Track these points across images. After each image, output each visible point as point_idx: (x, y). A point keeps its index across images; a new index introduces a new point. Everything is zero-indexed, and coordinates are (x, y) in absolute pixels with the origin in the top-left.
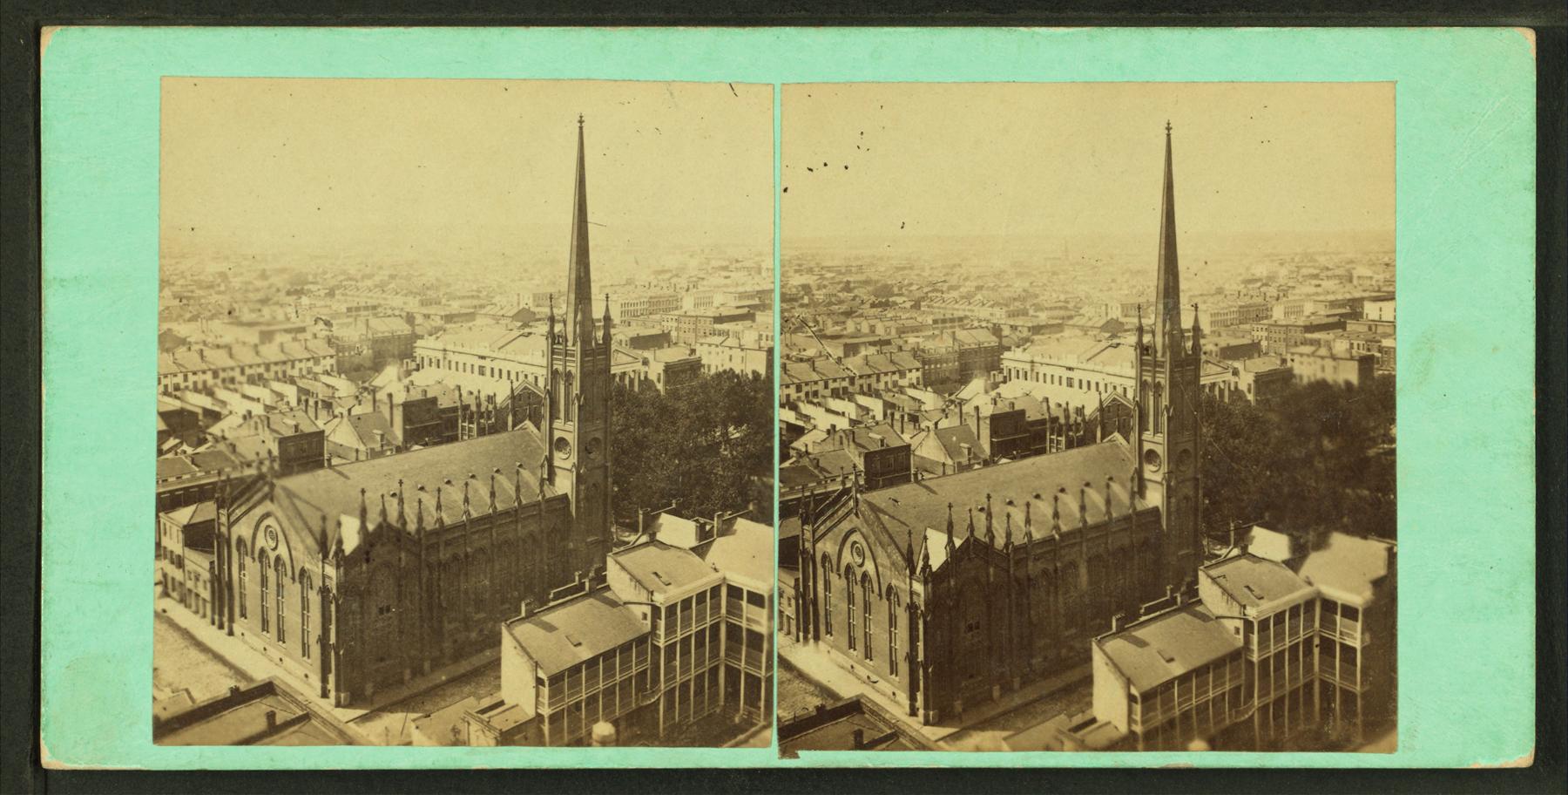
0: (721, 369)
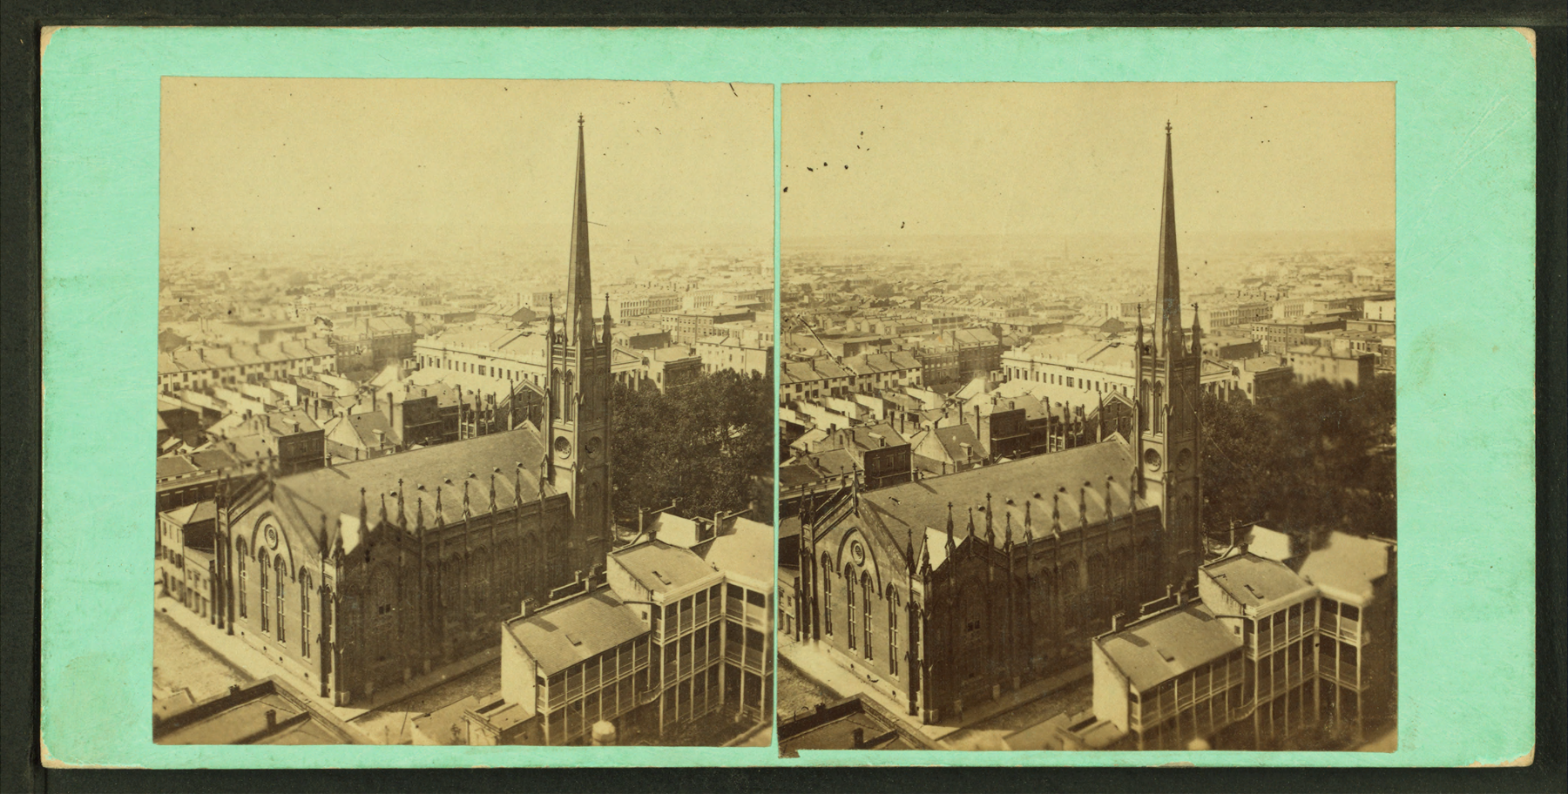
0: (721, 369)
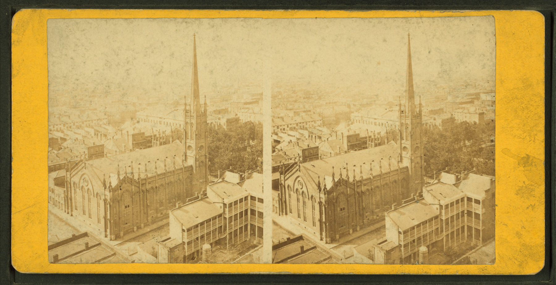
0: (462, 121)
